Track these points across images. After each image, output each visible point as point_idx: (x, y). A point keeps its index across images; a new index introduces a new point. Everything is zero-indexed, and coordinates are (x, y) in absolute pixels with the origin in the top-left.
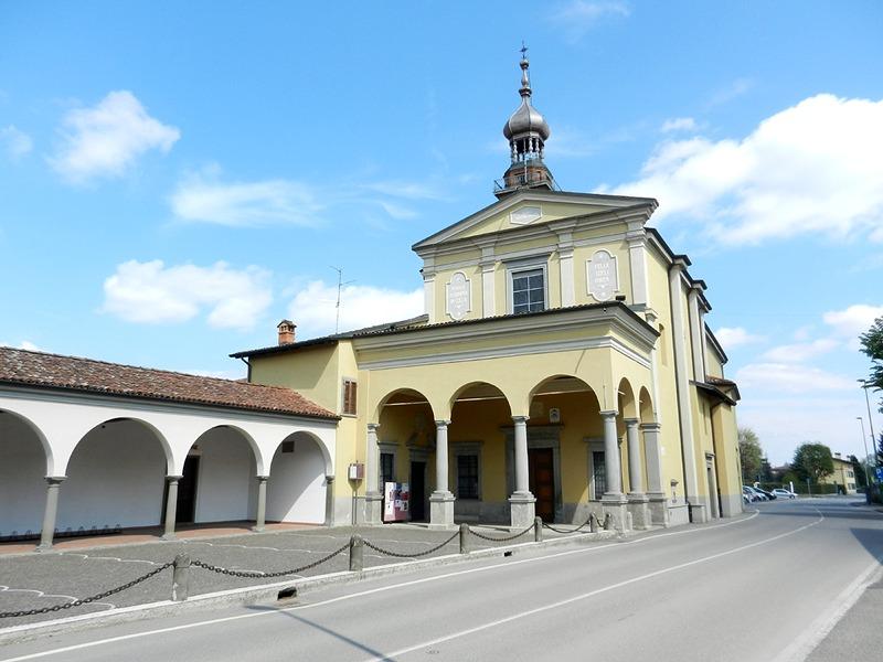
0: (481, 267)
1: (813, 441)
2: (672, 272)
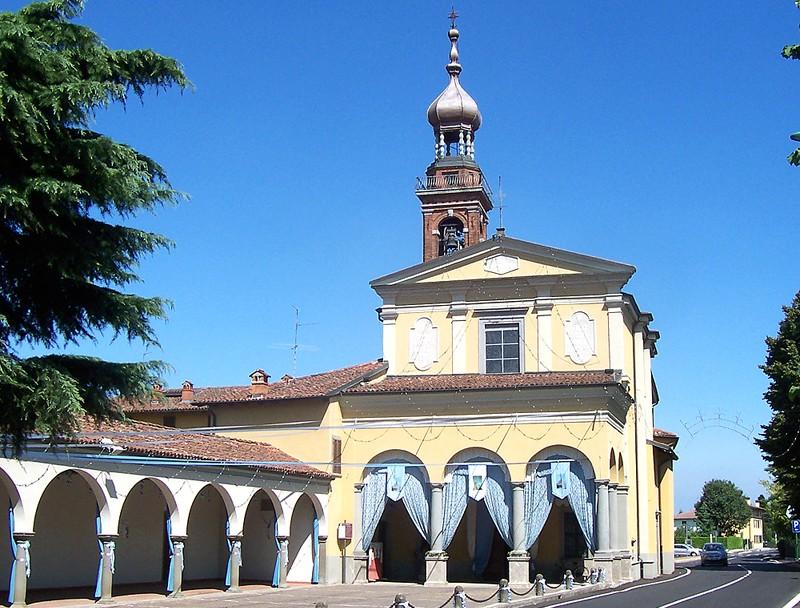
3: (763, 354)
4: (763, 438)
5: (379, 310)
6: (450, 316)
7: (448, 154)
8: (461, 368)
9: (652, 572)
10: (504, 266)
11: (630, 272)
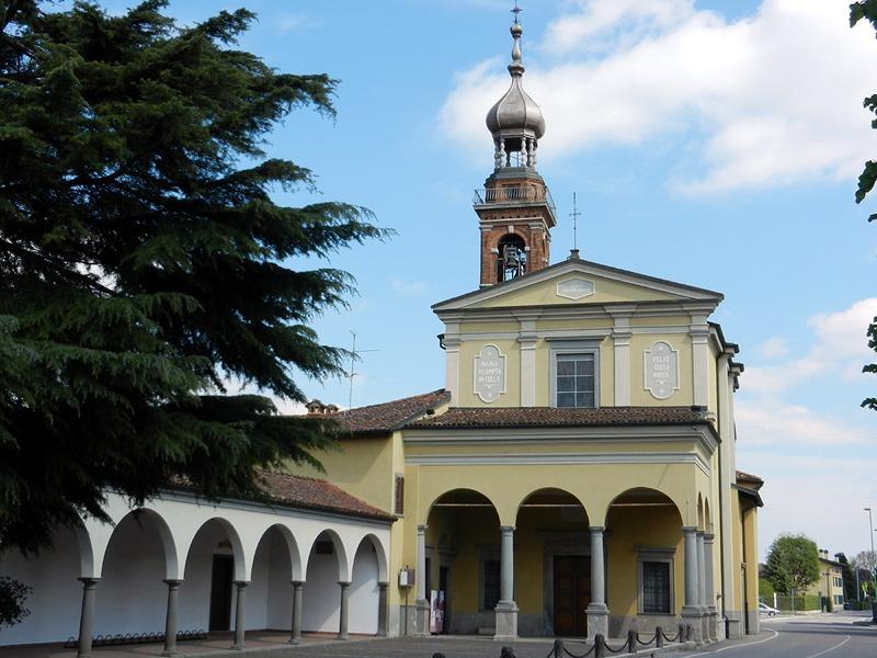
0: (519, 342)
1: (794, 533)
2: (720, 360)
8: (530, 401)
11: (716, 298)
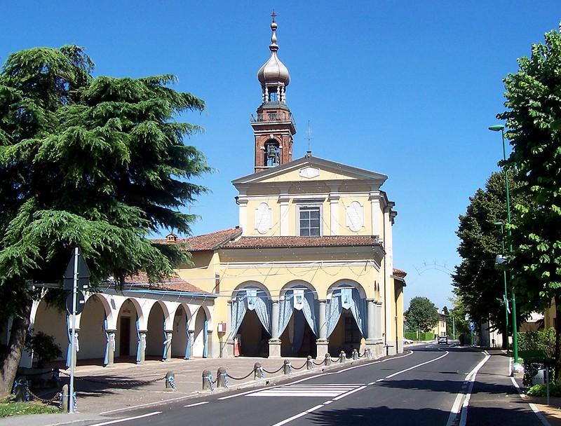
3: (458, 223)
4: (456, 274)
5: (237, 198)
6: (279, 202)
7: (269, 100)
9: (392, 352)
10: (311, 174)
